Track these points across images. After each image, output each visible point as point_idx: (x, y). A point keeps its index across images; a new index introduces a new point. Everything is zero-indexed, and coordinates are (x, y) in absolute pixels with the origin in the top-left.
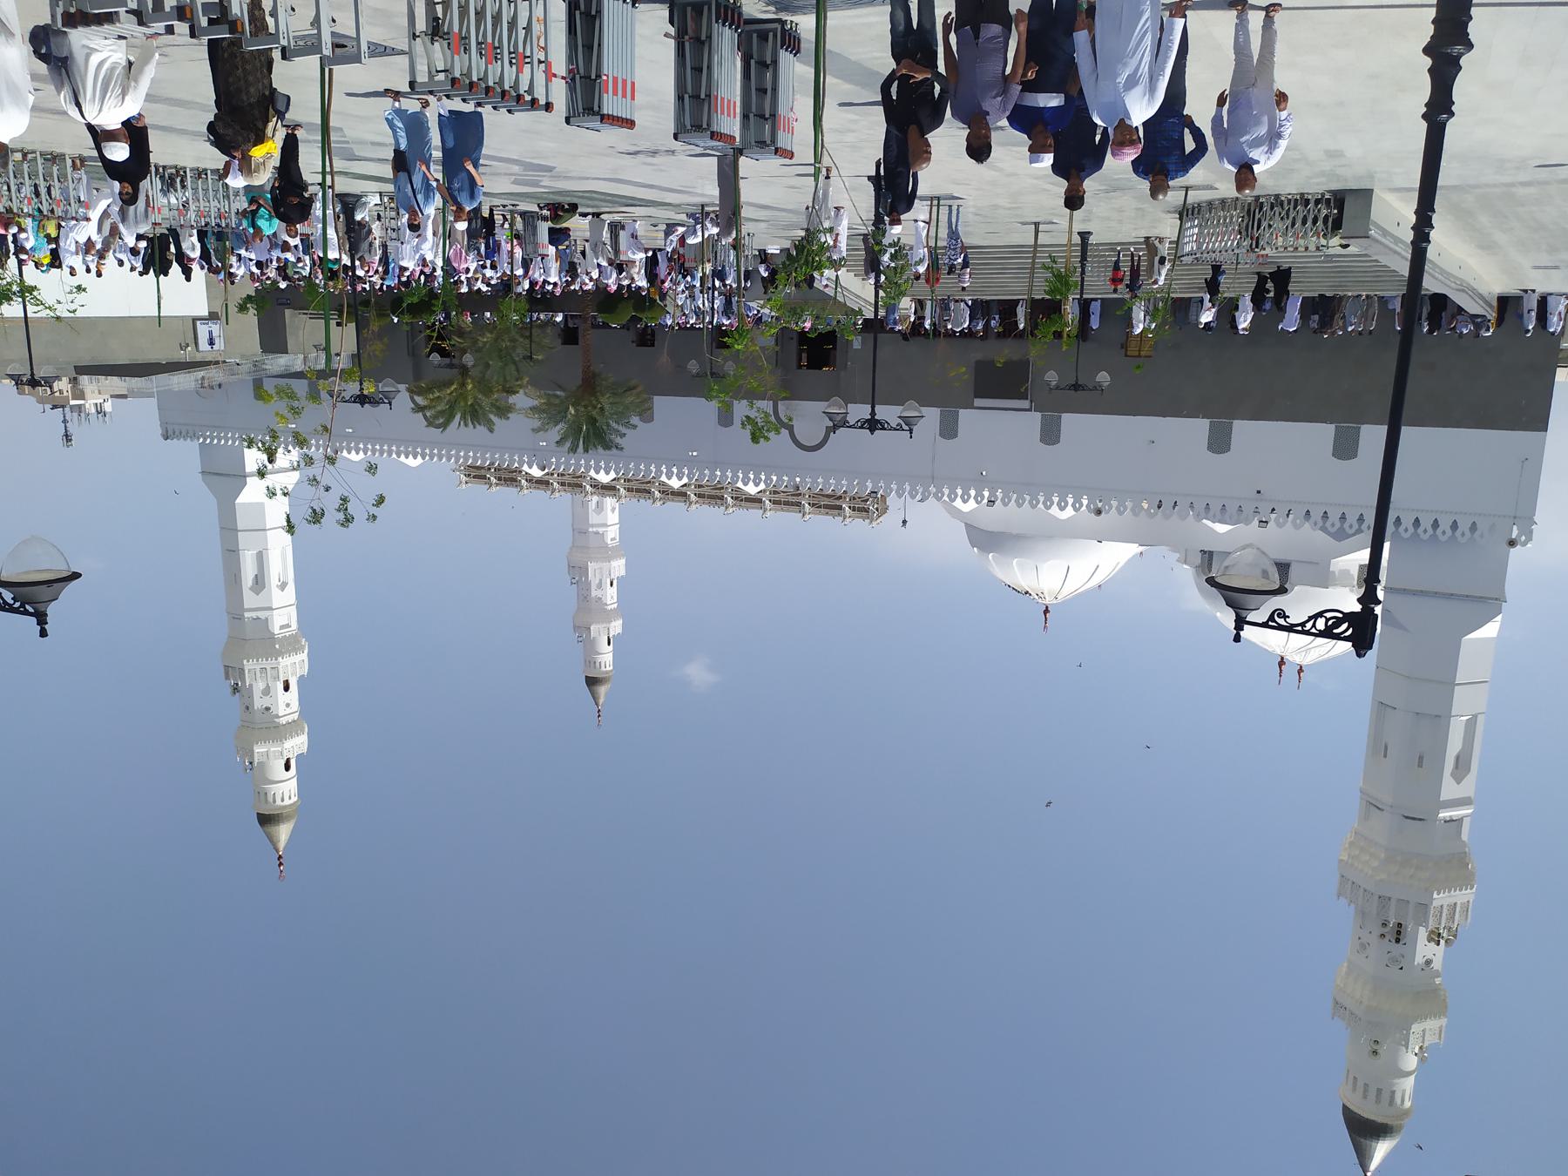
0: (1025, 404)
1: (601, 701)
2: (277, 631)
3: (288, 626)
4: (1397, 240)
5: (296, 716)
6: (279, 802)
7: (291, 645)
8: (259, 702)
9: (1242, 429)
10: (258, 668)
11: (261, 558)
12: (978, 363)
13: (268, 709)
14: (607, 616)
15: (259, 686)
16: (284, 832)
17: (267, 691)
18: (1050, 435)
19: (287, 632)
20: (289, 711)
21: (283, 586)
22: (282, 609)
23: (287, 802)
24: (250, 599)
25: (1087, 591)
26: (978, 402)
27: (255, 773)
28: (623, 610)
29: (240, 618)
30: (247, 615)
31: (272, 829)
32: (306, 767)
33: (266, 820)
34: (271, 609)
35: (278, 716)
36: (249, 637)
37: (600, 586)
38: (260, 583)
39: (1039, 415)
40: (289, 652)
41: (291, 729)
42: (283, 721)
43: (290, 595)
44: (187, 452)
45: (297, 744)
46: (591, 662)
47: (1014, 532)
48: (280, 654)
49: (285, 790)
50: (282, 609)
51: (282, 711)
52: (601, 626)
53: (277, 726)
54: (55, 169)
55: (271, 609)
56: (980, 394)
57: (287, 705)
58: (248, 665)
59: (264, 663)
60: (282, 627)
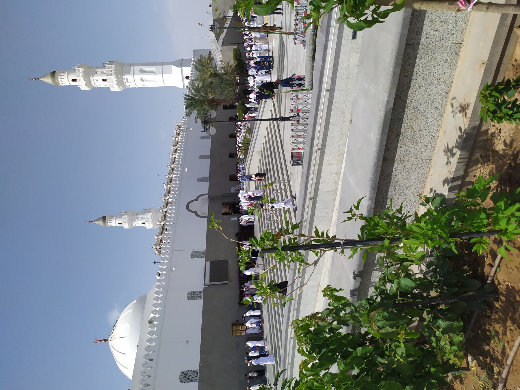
0: (208, 281)
1: (96, 222)
2: (126, 76)
3: (127, 81)
4: (298, 310)
5: (93, 84)
6: (60, 77)
7: (120, 83)
8: (99, 71)
10: (112, 69)
13: (96, 73)
14: (130, 222)
15: (105, 71)
16: (100, 223)
18: (192, 296)
19: (125, 81)
20: (95, 81)
21: (142, 80)
22: (134, 80)
23: (59, 80)
24: (137, 68)
25: (110, 349)
26: (208, 263)
28: (95, 90)
29: (131, 65)
30: (132, 67)
31: (101, 220)
32: (119, 228)
33: (104, 218)
34: (134, 75)
35: (93, 76)
36: (123, 69)
37: (142, 218)
38: (143, 72)
39: (202, 289)
40: (117, 80)
41: (88, 83)
42: (91, 78)
43: (140, 85)
44: (190, 56)
45: (126, 226)
46: (112, 217)
47: (146, 306)
48: (117, 77)
49: (113, 223)
50: (134, 80)
52: (126, 219)
55: (134, 75)
57: (97, 81)
58: (113, 66)
59: (113, 72)
60: (127, 79)
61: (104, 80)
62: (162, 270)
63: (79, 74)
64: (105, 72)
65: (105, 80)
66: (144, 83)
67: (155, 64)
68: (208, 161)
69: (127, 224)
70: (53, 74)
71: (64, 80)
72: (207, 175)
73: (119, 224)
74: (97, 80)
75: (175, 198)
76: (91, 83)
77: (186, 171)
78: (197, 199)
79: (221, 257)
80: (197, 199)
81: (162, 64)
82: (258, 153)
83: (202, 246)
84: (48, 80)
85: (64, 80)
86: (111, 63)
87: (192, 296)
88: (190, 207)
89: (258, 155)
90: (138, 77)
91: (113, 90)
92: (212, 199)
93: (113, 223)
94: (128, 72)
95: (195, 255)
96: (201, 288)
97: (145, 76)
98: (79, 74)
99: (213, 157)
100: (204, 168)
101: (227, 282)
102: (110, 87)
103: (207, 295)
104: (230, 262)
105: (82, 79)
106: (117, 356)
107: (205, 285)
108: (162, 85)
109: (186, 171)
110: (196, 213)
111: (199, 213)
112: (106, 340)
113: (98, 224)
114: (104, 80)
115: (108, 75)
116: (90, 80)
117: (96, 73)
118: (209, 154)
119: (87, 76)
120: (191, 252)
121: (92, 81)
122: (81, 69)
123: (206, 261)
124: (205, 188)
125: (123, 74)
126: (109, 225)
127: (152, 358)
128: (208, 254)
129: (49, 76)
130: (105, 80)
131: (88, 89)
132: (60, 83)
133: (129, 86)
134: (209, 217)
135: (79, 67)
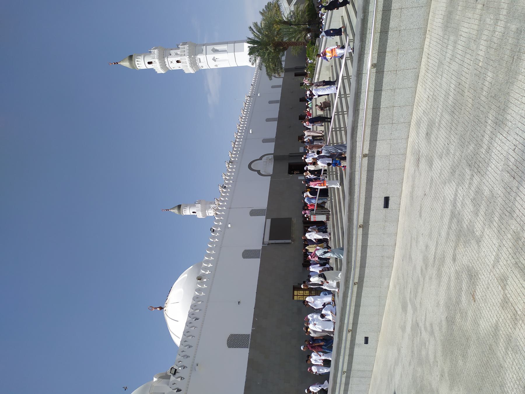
0: (267, 239)
1: (172, 211)
2: (199, 56)
5: (167, 66)
6: (136, 60)
7: (193, 63)
8: (173, 52)
9: (242, 355)
11: (225, 51)
12: (289, 220)
13: (170, 55)
14: (204, 211)
16: (176, 211)
17: (177, 54)
19: (198, 61)
20: (170, 62)
21: (214, 60)
23: (136, 63)
24: (210, 48)
26: (269, 221)
27: (193, 204)
28: (171, 74)
29: (204, 45)
30: (205, 47)
31: (177, 208)
32: (193, 218)
33: (179, 207)
34: (206, 54)
36: (195, 50)
38: (215, 51)
39: (260, 248)
40: (191, 61)
41: (163, 65)
42: (166, 60)
45: (200, 215)
48: (190, 57)
49: (187, 212)
50: (207, 61)
51: (170, 59)
53: (164, 58)
54: (338, 168)
56: (273, 221)
57: (172, 64)
58: (186, 46)
59: (186, 53)
60: (199, 59)
61: (178, 62)
62: (217, 226)
63: (154, 56)
64: (179, 53)
65: (179, 62)
66: (216, 63)
67: (227, 43)
68: (275, 123)
69: (200, 213)
70: (131, 58)
71: (141, 64)
72: (273, 135)
73: (193, 212)
74: (172, 62)
75: (237, 157)
76: (166, 65)
77: (251, 132)
78: (261, 159)
79: (284, 215)
80: (261, 159)
81: (235, 42)
82: (328, 69)
83: (263, 204)
84: (126, 64)
85: (141, 64)
86: (184, 44)
87: (248, 254)
88: (252, 166)
89: (328, 72)
90: (210, 57)
91: (186, 72)
92: (277, 159)
93: (187, 212)
94: (201, 52)
95: (254, 213)
96: (259, 247)
97: (217, 56)
98: (154, 56)
99: (280, 119)
100: (271, 130)
101: (289, 241)
102: (184, 69)
103: (266, 255)
104: (294, 220)
105: (157, 61)
106: (171, 324)
107: (263, 243)
108: (234, 65)
109: (251, 132)
110: (259, 172)
111: (261, 172)
112: (161, 308)
113: (174, 213)
114: (178, 62)
115: (181, 55)
116: (165, 62)
117: (170, 55)
118: (277, 117)
119: (162, 57)
120: (251, 209)
121: (167, 63)
122: (156, 51)
123: (266, 219)
124: (270, 148)
125: (196, 55)
126: (184, 214)
127: (198, 317)
128: (268, 212)
129: (127, 59)
130: (179, 62)
131: (163, 72)
132: (137, 66)
133: (202, 67)
134: (273, 176)
135: (155, 49)
